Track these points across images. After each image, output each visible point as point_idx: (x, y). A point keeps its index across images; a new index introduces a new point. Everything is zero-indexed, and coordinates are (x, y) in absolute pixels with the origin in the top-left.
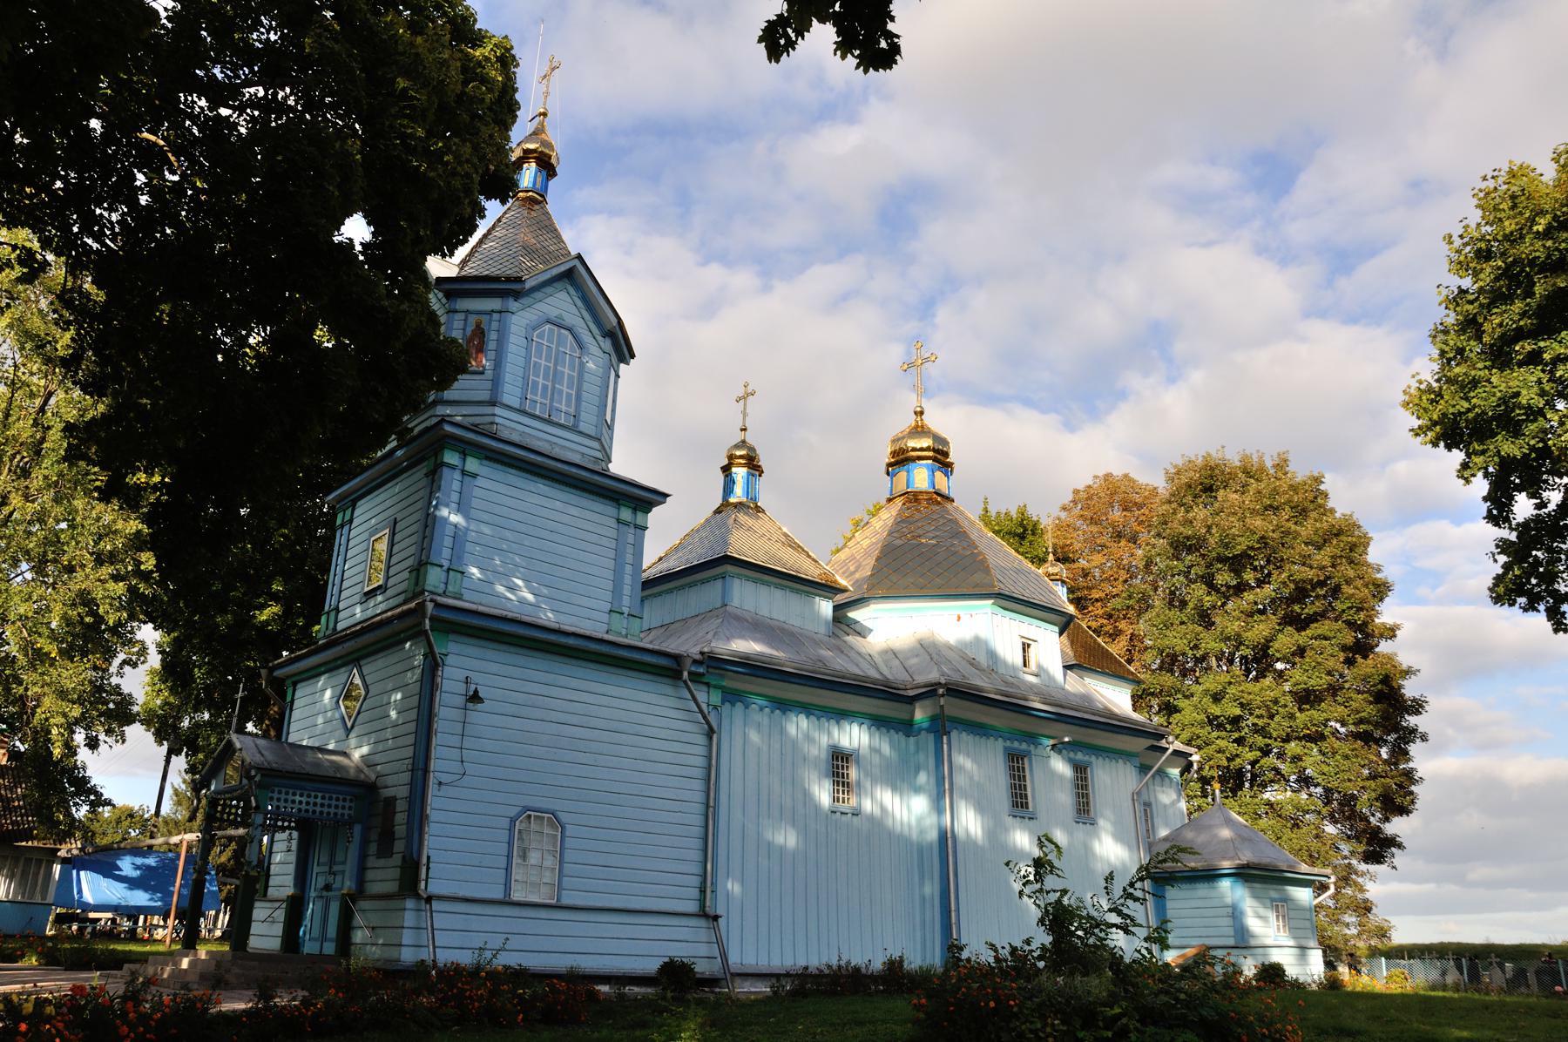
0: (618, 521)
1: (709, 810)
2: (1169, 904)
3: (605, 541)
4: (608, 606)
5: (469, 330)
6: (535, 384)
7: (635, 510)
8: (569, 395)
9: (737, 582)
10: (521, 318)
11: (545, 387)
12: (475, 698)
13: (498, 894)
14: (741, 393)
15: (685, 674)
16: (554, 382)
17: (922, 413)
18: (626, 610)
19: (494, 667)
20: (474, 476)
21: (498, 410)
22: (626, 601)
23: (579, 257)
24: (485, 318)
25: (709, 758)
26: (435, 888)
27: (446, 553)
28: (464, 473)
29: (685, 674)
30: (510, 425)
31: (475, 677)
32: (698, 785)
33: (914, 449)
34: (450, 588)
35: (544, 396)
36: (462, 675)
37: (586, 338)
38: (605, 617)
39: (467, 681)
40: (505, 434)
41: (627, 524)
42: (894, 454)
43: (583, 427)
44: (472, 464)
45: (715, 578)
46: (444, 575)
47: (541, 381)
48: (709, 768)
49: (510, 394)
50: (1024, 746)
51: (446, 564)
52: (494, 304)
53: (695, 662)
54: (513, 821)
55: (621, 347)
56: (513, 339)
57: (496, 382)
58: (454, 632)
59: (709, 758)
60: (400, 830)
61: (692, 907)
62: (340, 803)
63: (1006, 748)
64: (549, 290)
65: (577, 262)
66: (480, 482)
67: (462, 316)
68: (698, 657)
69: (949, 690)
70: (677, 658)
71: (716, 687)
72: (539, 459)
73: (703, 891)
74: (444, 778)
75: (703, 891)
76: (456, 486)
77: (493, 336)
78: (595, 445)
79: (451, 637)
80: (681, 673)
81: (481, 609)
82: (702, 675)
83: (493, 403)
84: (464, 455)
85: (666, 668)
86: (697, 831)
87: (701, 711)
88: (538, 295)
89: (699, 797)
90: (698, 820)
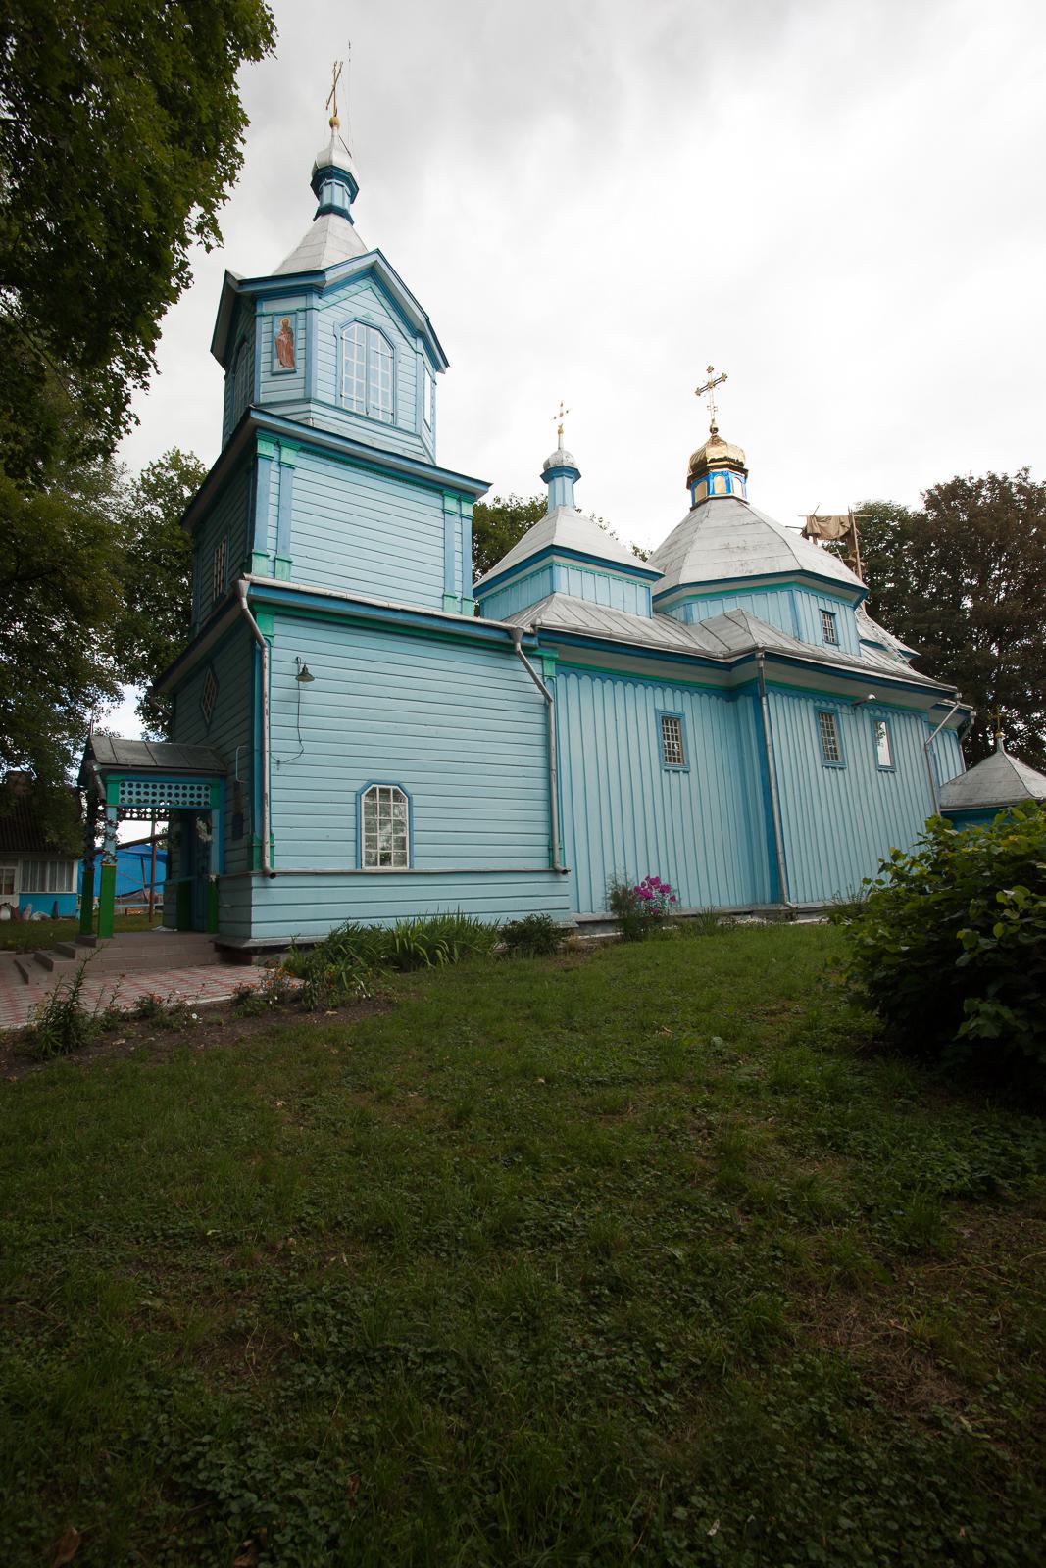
0: (444, 511)
6: (376, 391)
7: (459, 500)
8: (385, 394)
10: (327, 316)
12: (304, 676)
13: (350, 867)
15: (518, 645)
16: (368, 386)
17: (716, 430)
20: (293, 467)
21: (313, 407)
22: (458, 586)
23: (378, 251)
24: (290, 318)
25: (547, 724)
26: (280, 864)
28: (281, 464)
29: (518, 645)
30: (323, 419)
31: (305, 657)
32: (539, 751)
33: (713, 460)
35: (359, 393)
38: (439, 602)
39: (297, 661)
41: (453, 514)
43: (401, 424)
44: (289, 455)
45: (542, 570)
46: (271, 564)
49: (323, 390)
50: (831, 706)
52: (297, 303)
53: (526, 635)
54: (358, 794)
55: (438, 361)
56: (320, 336)
57: (307, 380)
59: (547, 724)
60: (554, 768)
63: (815, 708)
64: (353, 288)
65: (376, 257)
66: (298, 473)
67: (268, 319)
68: (529, 630)
69: (766, 653)
70: (508, 632)
71: (550, 659)
72: (357, 448)
74: (283, 757)
76: (274, 477)
77: (300, 334)
78: (417, 441)
80: (513, 646)
81: (303, 588)
83: (308, 400)
84: (278, 445)
85: (500, 645)
86: (541, 793)
87: (537, 681)
88: (342, 293)
89: (540, 761)
90: (541, 783)
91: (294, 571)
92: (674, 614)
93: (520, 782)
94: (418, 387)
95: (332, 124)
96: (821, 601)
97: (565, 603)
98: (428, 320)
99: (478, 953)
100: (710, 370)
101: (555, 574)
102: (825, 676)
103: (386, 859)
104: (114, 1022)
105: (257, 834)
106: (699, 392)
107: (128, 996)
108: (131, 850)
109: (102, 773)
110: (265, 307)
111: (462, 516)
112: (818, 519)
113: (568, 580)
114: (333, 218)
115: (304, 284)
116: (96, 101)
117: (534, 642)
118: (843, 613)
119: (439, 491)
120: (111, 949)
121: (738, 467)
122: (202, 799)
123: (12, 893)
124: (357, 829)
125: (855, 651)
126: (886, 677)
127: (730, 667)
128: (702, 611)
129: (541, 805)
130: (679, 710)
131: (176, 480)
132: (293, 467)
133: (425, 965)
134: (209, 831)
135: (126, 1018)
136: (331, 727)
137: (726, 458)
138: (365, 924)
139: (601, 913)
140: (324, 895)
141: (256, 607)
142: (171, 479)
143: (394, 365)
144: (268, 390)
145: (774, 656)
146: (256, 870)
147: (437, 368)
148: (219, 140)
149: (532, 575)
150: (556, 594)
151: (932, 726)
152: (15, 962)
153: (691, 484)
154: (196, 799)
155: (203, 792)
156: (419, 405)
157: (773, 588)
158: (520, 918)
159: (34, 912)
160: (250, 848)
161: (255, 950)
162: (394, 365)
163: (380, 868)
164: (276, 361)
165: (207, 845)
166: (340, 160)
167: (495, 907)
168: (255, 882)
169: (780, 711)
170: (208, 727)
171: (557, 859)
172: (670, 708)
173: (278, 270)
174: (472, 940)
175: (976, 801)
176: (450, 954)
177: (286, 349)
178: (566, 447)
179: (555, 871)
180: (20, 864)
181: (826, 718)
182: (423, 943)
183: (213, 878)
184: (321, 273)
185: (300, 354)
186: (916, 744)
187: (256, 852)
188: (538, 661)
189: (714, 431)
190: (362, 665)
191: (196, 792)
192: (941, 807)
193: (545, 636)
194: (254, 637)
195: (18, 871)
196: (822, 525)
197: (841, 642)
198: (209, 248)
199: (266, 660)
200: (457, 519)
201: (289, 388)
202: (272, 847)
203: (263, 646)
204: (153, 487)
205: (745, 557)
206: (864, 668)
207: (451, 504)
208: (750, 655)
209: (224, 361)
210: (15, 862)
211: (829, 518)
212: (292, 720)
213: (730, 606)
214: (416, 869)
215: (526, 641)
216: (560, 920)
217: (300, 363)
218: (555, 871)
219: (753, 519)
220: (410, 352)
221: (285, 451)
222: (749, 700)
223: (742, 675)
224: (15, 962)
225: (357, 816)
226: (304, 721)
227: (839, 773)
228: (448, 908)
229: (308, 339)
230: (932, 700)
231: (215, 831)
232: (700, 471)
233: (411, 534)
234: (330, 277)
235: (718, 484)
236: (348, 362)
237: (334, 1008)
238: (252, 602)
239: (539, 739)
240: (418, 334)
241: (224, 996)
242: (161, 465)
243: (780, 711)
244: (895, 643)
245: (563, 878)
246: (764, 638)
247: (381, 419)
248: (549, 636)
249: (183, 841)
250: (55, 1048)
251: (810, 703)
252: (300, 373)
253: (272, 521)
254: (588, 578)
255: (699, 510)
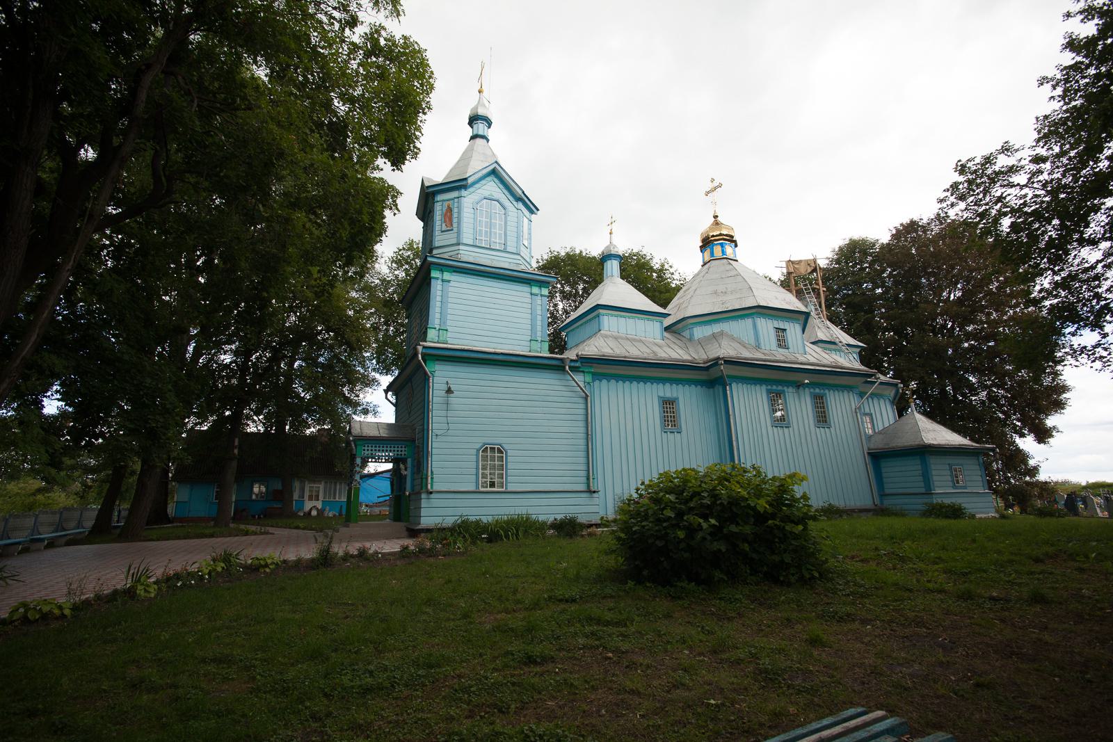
1: (588, 436)
2: (884, 470)
3: (525, 305)
4: (529, 338)
5: (444, 209)
6: (495, 233)
8: (500, 234)
9: (606, 318)
10: (469, 199)
11: (486, 232)
12: (449, 391)
13: (472, 488)
14: (709, 186)
15: (567, 367)
16: (490, 228)
17: (717, 216)
18: (539, 339)
19: (462, 375)
20: (449, 281)
21: (461, 247)
22: (539, 334)
23: (496, 162)
26: (437, 487)
27: (437, 321)
28: (443, 281)
29: (567, 367)
30: (467, 255)
32: (582, 424)
33: (713, 236)
34: (441, 338)
35: (486, 236)
36: (445, 380)
37: (507, 203)
40: (463, 259)
41: (537, 295)
42: (703, 241)
43: (509, 249)
44: (447, 276)
45: (595, 317)
47: (484, 229)
48: (587, 415)
49: (467, 238)
50: (780, 388)
51: (438, 327)
53: (572, 361)
55: (532, 208)
56: (465, 210)
57: (459, 233)
58: (438, 360)
61: (582, 487)
62: (400, 449)
63: (767, 389)
64: (483, 182)
65: (495, 165)
66: (452, 284)
69: (725, 361)
70: (562, 360)
72: (482, 268)
73: (588, 479)
74: (439, 432)
75: (588, 479)
76: (439, 287)
77: (456, 210)
79: (437, 362)
80: (564, 367)
82: (579, 367)
85: (558, 367)
86: (583, 447)
88: (477, 186)
89: (583, 430)
90: (583, 442)
91: (449, 334)
92: (684, 334)
93: (565, 442)
94: (519, 226)
95: (480, 92)
96: (775, 322)
97: (606, 336)
98: (523, 192)
99: (532, 535)
100: (713, 180)
101: (601, 320)
102: (775, 371)
103: (492, 485)
104: (347, 557)
105: (425, 472)
106: (707, 193)
107: (353, 549)
108: (384, 475)
109: (354, 441)
110: (439, 197)
111: (542, 295)
112: (793, 262)
113: (609, 323)
114: (479, 141)
115: (457, 185)
116: (311, 360)
117: (578, 364)
118: (792, 329)
119: (529, 284)
120: (354, 529)
121: (731, 240)
122: (403, 453)
123: (318, 500)
124: (477, 468)
125: (801, 351)
126: (818, 368)
127: (707, 369)
128: (700, 332)
129: (583, 454)
130: (675, 395)
131: (412, 256)
132: (449, 281)
133: (502, 539)
134: (406, 469)
135: (352, 556)
136: (466, 412)
137: (721, 235)
138: (472, 519)
139: (611, 516)
140: (525, 502)
141: (427, 358)
142: (409, 256)
143: (506, 218)
144: (439, 239)
145: (729, 362)
146: (424, 490)
147: (532, 212)
148: (410, 143)
149: (590, 320)
150: (602, 332)
151: (862, 395)
152: (315, 536)
153: (703, 248)
154: (400, 453)
155: (403, 449)
156: (519, 237)
157: (742, 317)
158: (559, 517)
159: (329, 511)
160: (422, 478)
161: (423, 530)
162: (506, 218)
163: (489, 489)
164: (444, 225)
165: (1051, 305)
166: (481, 112)
167: (547, 511)
168: (423, 496)
169: (741, 397)
170: (409, 414)
171: (591, 485)
172: (668, 395)
173: (445, 178)
174: (530, 527)
175: (891, 446)
176: (517, 535)
177: (448, 215)
178: (614, 243)
179: (591, 492)
180: (323, 483)
181: (775, 398)
182: (502, 528)
183: (407, 493)
184: (466, 179)
185: (455, 220)
186: (848, 408)
187: (424, 480)
188: (582, 374)
189: (716, 217)
190: (482, 383)
191: (400, 449)
192: (869, 449)
193: (584, 361)
194: (426, 373)
195: (322, 486)
196: (796, 266)
197: (790, 346)
198: (395, 214)
199: (431, 384)
200: (539, 297)
201: (449, 238)
202: (432, 478)
203: (429, 377)
204: (399, 261)
205: (725, 298)
206: (801, 364)
207: (535, 290)
208: (716, 362)
209: (422, 219)
210: (320, 482)
211: (800, 261)
212: (444, 413)
213: (716, 328)
214: (509, 489)
215: (572, 364)
216: (582, 519)
217: (455, 225)
218: (591, 492)
219: (735, 273)
220: (513, 207)
221: (445, 273)
222: (721, 389)
223: (714, 373)
224: (315, 536)
225: (477, 462)
226: (450, 413)
227: (786, 430)
228: (522, 511)
229: (459, 213)
230: (863, 379)
231: (409, 470)
232: (707, 243)
233: (513, 309)
234: (470, 181)
235: (717, 251)
236: (480, 221)
237: (444, 556)
238: (424, 355)
239: (582, 417)
240: (519, 199)
241: (397, 549)
242: (404, 249)
243: (741, 397)
244: (846, 339)
245: (595, 495)
246: (727, 350)
247: (498, 248)
248: (586, 362)
249: (396, 477)
250: (321, 564)
251: (764, 387)
252: (455, 230)
253: (438, 310)
254: (622, 320)
255: (707, 266)
